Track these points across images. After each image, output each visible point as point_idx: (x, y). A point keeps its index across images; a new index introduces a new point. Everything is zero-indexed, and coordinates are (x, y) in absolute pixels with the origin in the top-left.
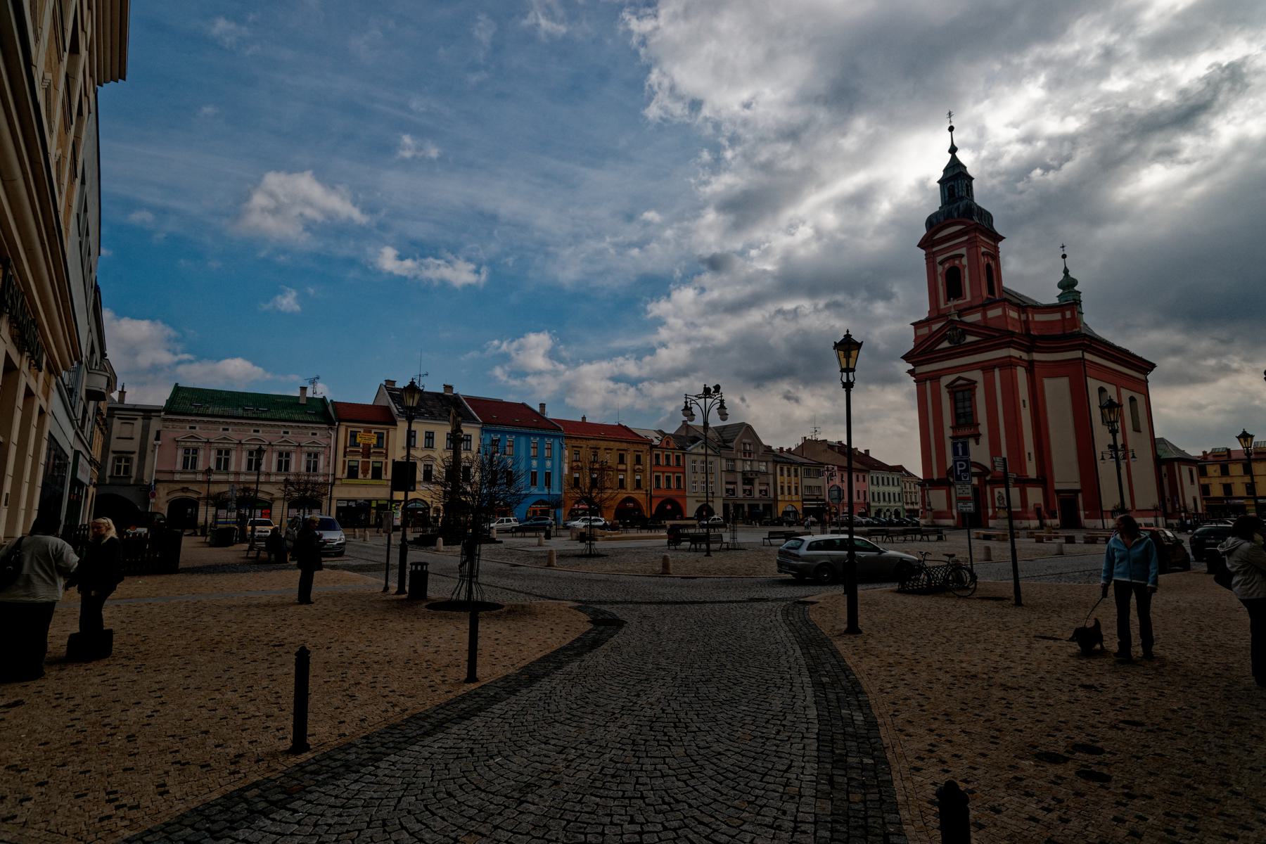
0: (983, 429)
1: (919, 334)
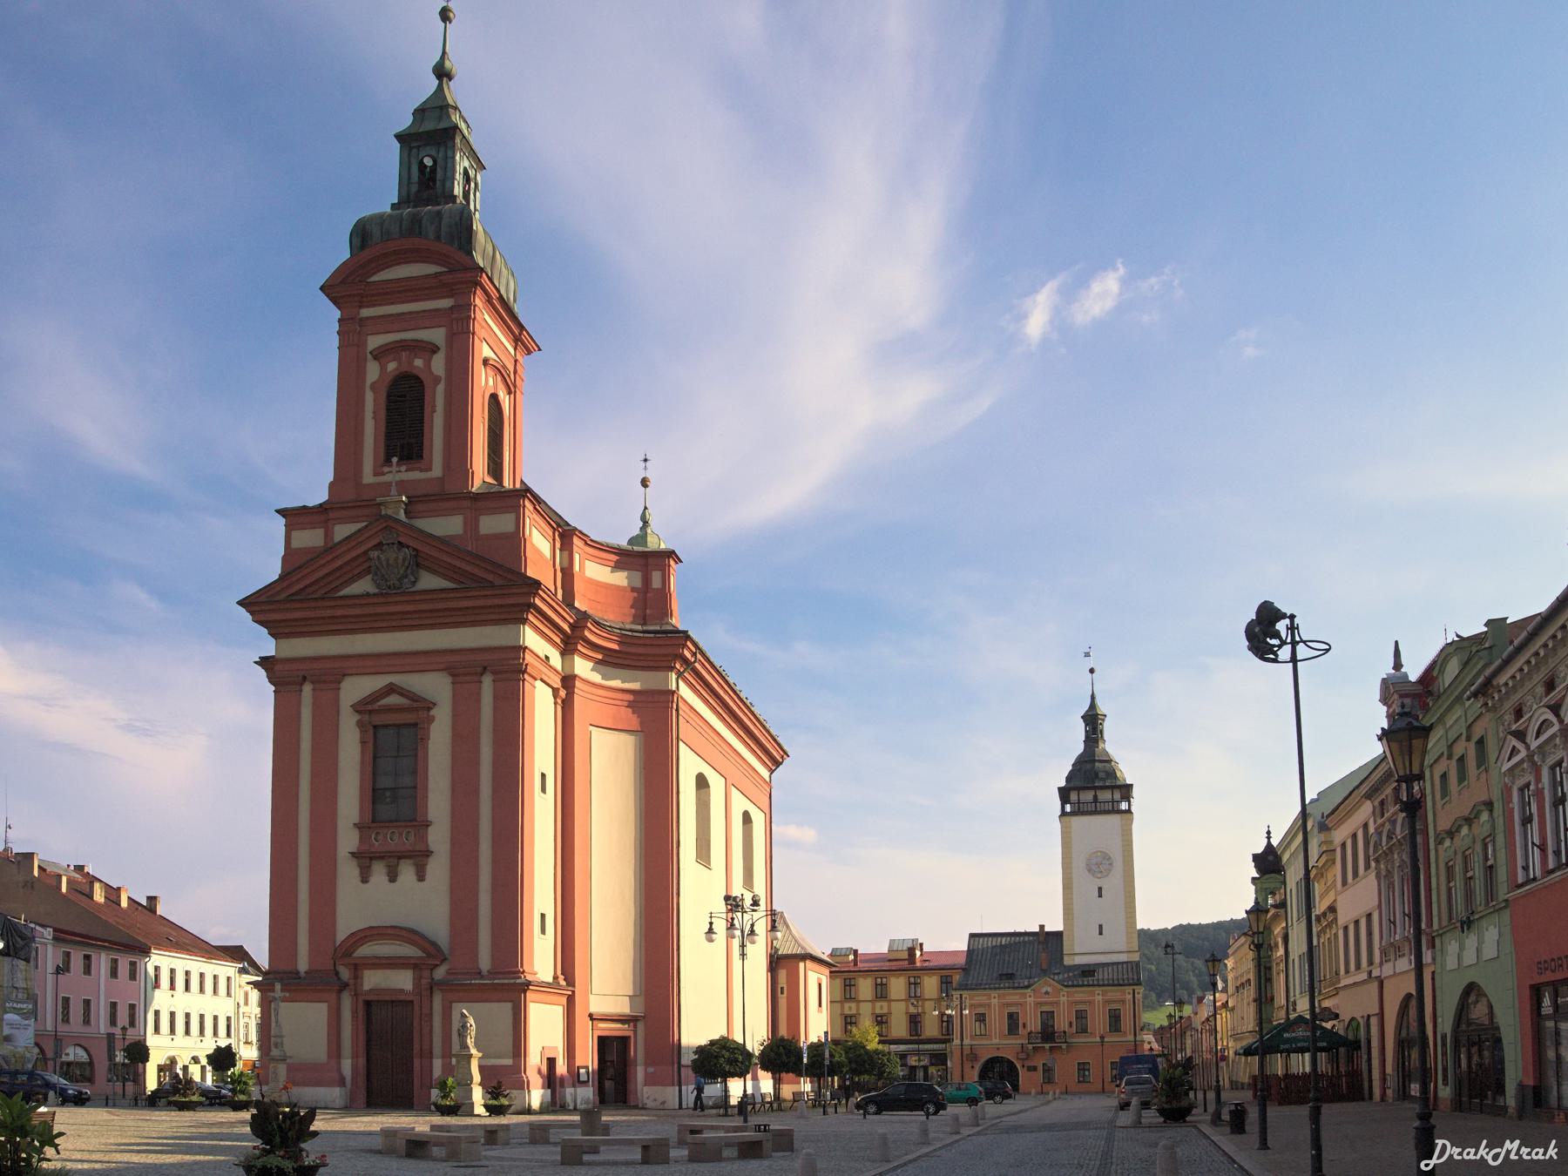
0: (439, 837)
1: (295, 544)
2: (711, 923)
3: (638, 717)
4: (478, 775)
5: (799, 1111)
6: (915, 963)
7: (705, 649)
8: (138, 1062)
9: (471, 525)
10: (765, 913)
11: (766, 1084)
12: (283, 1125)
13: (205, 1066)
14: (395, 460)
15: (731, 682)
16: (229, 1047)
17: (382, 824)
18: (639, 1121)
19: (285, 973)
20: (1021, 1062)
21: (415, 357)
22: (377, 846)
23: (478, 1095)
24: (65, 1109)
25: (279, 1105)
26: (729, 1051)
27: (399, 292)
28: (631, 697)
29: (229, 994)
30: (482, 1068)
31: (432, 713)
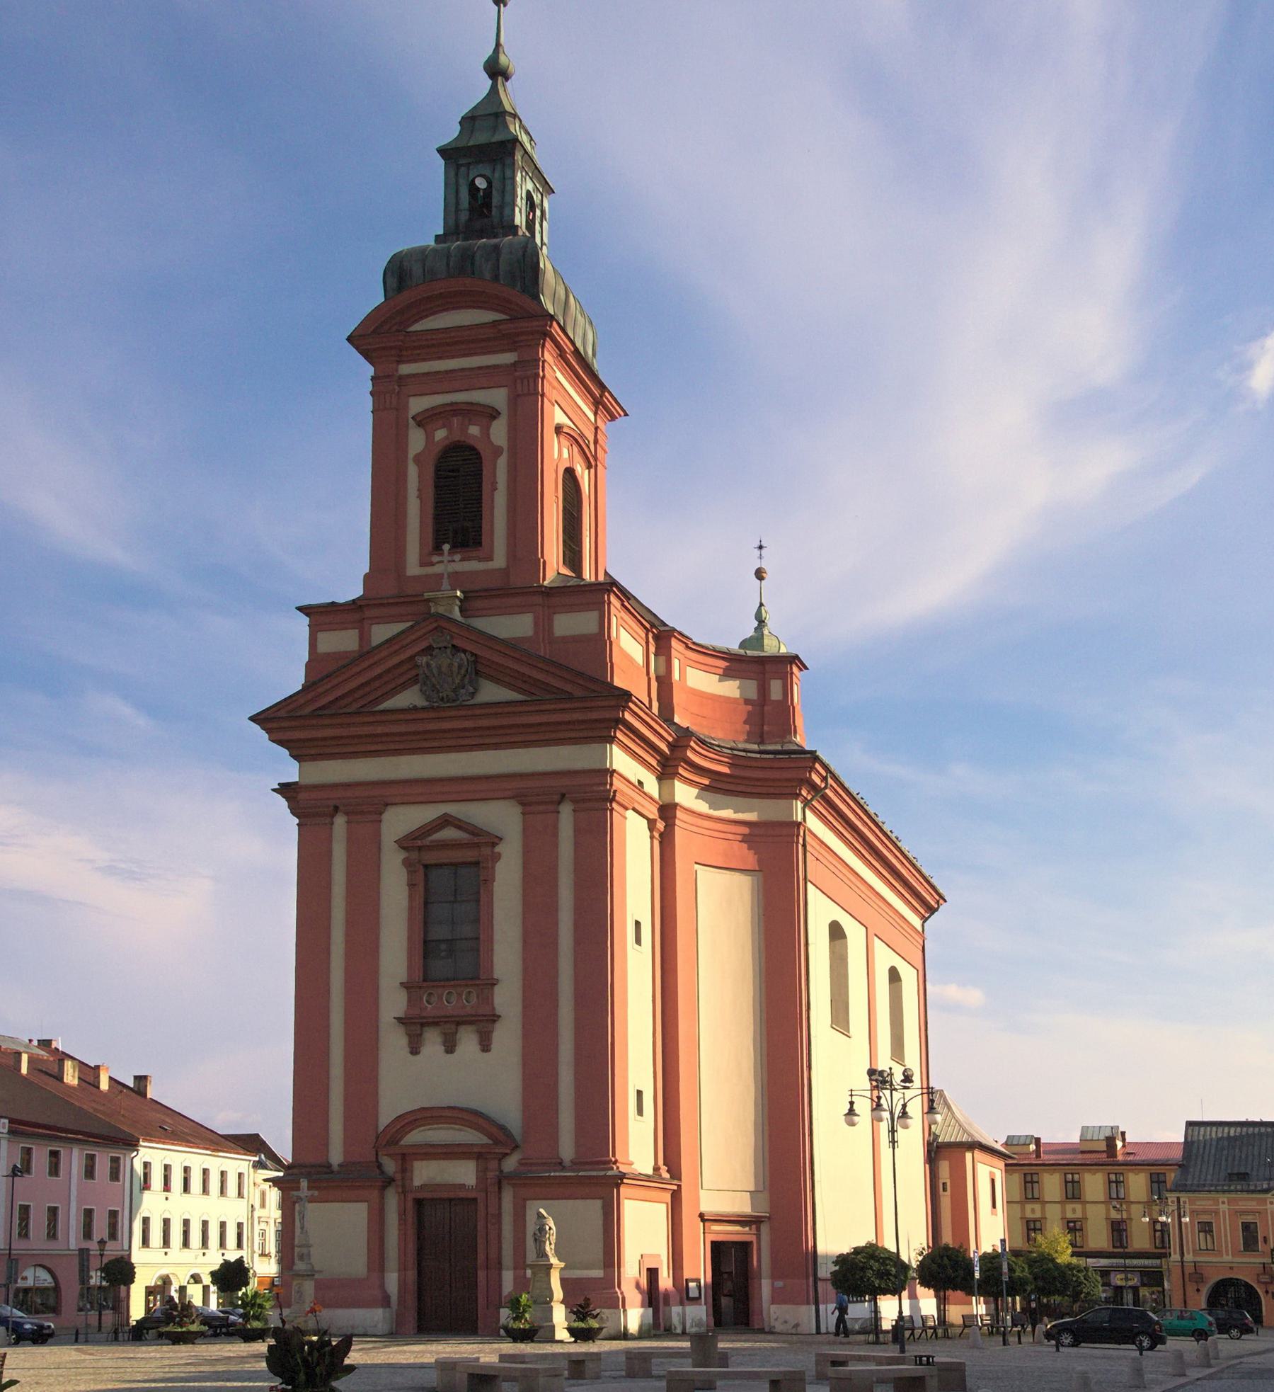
2: (852, 1103)
3: (755, 854)
4: (556, 924)
5: (971, 1339)
6: (1116, 1157)
7: (837, 772)
8: (120, 1285)
9: (543, 625)
10: (920, 1091)
11: (928, 1304)
12: (310, 1359)
13: (208, 1286)
14: (446, 547)
15: (871, 811)
16: (240, 1261)
17: (435, 983)
18: (765, 1348)
19: (312, 1166)
20: (1263, 1286)
21: (470, 424)
22: (430, 1010)
23: (559, 1315)
24: (19, 1350)
25: (304, 1333)
26: (878, 1261)
27: (448, 344)
28: (746, 830)
29: (240, 1195)
30: (564, 1282)
31: (497, 849)
